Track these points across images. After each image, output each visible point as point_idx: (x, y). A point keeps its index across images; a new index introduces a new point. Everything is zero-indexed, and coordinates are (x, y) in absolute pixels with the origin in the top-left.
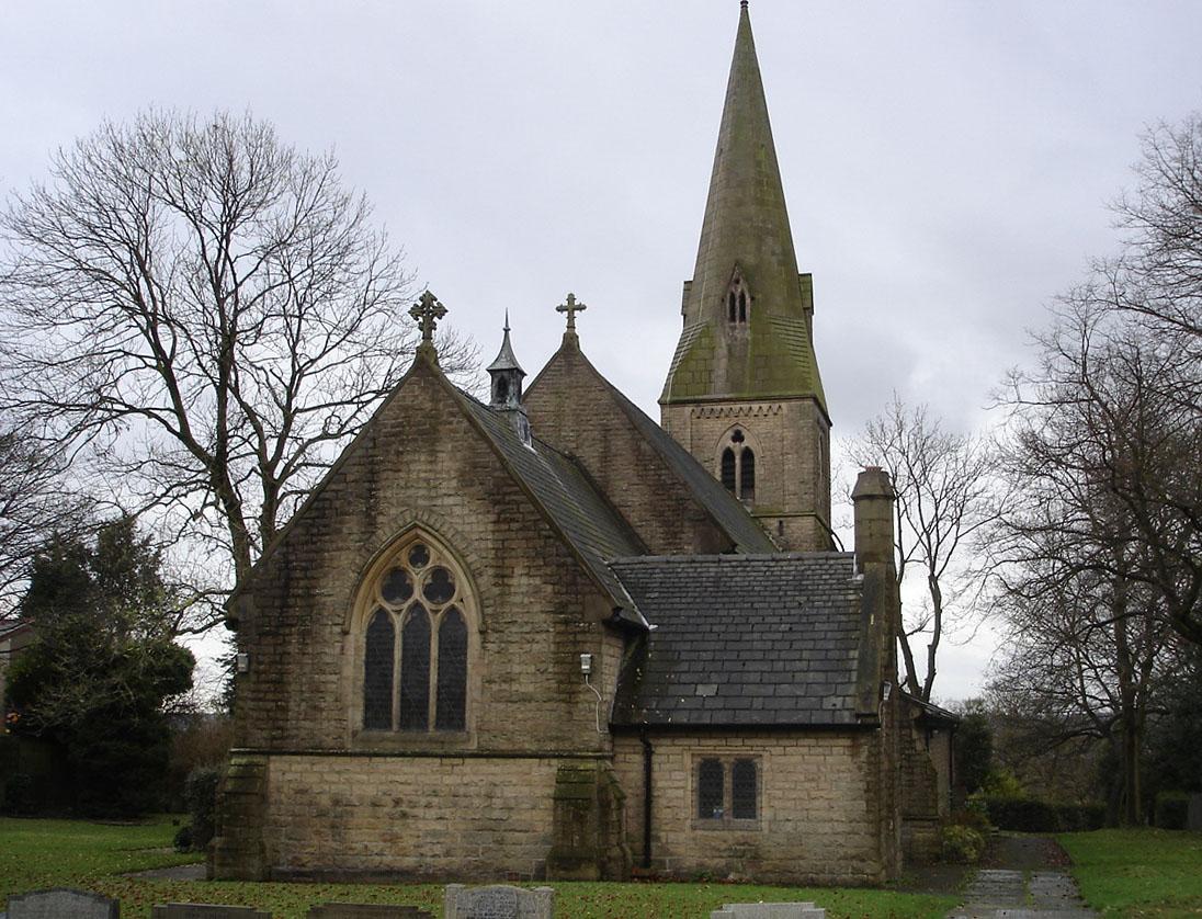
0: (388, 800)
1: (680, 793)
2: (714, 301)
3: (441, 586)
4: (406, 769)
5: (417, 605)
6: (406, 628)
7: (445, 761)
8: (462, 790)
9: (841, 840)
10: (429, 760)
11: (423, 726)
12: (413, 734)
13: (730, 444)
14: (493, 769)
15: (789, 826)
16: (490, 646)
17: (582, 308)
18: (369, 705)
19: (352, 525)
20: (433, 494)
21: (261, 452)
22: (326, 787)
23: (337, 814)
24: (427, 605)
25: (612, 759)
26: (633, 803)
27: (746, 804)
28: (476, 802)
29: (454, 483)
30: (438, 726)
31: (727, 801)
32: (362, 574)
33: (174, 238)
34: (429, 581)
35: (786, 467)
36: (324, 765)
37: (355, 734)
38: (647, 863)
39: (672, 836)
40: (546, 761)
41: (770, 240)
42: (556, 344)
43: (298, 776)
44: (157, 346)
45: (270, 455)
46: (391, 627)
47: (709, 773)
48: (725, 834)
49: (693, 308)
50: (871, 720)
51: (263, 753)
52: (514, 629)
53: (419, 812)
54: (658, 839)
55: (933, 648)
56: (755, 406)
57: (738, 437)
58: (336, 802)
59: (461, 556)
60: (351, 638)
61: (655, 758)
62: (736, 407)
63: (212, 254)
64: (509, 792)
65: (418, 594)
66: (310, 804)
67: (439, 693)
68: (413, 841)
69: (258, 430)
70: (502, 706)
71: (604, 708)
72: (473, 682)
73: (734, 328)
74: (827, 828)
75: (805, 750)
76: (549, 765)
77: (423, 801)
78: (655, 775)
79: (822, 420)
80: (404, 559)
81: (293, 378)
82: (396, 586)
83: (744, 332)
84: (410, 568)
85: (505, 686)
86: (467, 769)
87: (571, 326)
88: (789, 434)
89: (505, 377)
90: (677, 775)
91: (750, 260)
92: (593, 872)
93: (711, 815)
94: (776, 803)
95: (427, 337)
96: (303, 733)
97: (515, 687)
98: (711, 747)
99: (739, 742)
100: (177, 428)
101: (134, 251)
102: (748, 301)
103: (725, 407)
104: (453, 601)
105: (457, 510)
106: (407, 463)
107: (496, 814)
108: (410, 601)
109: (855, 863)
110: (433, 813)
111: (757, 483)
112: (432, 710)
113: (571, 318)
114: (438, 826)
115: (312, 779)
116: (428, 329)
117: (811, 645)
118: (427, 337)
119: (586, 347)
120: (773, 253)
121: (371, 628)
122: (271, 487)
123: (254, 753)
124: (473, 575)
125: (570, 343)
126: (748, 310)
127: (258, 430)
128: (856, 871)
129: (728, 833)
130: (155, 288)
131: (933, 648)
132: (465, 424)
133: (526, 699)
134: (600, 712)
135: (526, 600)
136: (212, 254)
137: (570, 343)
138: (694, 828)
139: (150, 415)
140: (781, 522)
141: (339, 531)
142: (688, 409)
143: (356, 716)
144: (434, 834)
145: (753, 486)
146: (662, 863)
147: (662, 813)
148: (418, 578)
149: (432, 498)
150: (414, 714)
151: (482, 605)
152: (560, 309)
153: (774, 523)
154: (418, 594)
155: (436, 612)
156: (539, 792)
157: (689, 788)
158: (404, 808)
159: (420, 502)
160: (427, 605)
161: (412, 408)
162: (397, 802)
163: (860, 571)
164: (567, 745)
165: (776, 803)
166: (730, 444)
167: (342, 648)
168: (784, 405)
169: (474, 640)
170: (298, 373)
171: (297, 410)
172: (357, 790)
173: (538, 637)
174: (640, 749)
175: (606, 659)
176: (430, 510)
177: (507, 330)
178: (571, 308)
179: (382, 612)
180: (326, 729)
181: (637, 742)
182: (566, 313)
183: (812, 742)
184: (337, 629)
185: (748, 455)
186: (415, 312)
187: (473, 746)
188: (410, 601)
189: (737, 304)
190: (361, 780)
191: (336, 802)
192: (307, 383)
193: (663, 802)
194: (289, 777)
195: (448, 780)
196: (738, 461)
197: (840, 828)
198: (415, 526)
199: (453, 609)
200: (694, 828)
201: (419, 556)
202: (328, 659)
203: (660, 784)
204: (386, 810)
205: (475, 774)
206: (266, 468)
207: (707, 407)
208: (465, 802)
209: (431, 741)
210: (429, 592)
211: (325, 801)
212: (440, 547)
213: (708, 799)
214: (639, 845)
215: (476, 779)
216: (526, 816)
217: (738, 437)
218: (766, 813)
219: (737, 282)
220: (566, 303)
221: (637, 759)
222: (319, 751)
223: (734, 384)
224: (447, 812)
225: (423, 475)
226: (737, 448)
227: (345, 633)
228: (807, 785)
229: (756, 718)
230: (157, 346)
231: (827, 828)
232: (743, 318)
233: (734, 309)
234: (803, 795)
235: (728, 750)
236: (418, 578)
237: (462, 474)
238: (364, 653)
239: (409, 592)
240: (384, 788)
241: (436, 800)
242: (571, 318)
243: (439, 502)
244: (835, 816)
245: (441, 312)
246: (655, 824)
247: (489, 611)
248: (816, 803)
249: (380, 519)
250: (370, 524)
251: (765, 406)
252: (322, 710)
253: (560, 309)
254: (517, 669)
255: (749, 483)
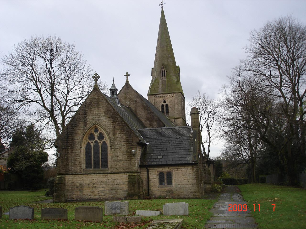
0: (92, 184)
1: (155, 180)
2: (158, 72)
3: (101, 137)
4: (95, 177)
5: (96, 141)
6: (94, 146)
7: (104, 175)
8: (108, 181)
9: (191, 188)
10: (100, 175)
11: (99, 167)
12: (96, 169)
13: (163, 103)
14: (114, 176)
15: (179, 186)
16: (112, 149)
17: (129, 75)
18: (87, 163)
19: (81, 124)
20: (99, 117)
21: (61, 109)
22: (78, 181)
23: (81, 187)
24: (98, 141)
25: (140, 173)
26: (145, 182)
27: (170, 181)
28: (111, 183)
29: (103, 114)
30: (102, 167)
31: (165, 181)
32: (84, 135)
33: (40, 63)
34: (99, 136)
35: (175, 108)
36: (77, 177)
37: (84, 169)
38: (149, 195)
39: (154, 189)
40: (126, 174)
41: (170, 59)
42: (124, 83)
43: (72, 179)
44: (37, 87)
45: (63, 110)
46: (91, 146)
47: (161, 175)
48: (165, 188)
49: (154, 74)
50: (196, 162)
51: (64, 175)
52: (118, 145)
53: (99, 186)
54: (151, 190)
55: (209, 146)
56: (168, 95)
57: (165, 102)
58: (80, 185)
59: (105, 130)
60: (82, 149)
61: (149, 172)
62: (164, 95)
63: (48, 66)
64: (118, 181)
65: (96, 139)
66: (75, 185)
67: (102, 160)
68: (97, 192)
69: (60, 104)
70: (116, 162)
71: (138, 162)
72: (109, 157)
73: (163, 78)
74: (187, 186)
75: (182, 169)
76: (126, 175)
77: (99, 184)
78: (150, 176)
79: (183, 97)
80: (93, 131)
81: (67, 93)
82: (92, 137)
83: (165, 79)
84: (94, 133)
85: (116, 158)
86: (109, 176)
87: (127, 79)
88: (176, 101)
89: (113, 91)
90: (154, 176)
91: (166, 63)
92: (137, 198)
93: (162, 184)
94: (176, 181)
95: (96, 83)
96: (73, 170)
97: (118, 158)
98: (161, 169)
99: (168, 168)
100: (42, 105)
101: (32, 66)
102: (166, 72)
103: (162, 95)
104: (104, 140)
105: (104, 120)
106: (93, 110)
107: (115, 186)
108: (95, 140)
109: (194, 193)
110: (101, 186)
111: (169, 112)
112: (100, 164)
113: (127, 77)
114: (103, 189)
115: (75, 180)
116: (96, 81)
117: (182, 146)
118: (96, 83)
119: (131, 84)
120: (171, 62)
121: (86, 146)
122: (63, 117)
123: (62, 175)
124: (108, 134)
125: (127, 83)
126: (166, 74)
127: (60, 104)
128: (194, 195)
129: (166, 188)
130: (36, 74)
131: (209, 146)
132: (105, 101)
133: (121, 160)
134: (137, 163)
135: (120, 139)
136: (48, 66)
137: (127, 83)
138: (158, 187)
139: (37, 102)
140: (175, 120)
141: (79, 126)
142: (154, 96)
143: (84, 166)
144: (102, 191)
145: (168, 112)
146: (152, 195)
147: (151, 184)
148: (96, 135)
149: (99, 118)
150: (96, 165)
151: (110, 141)
152: (125, 75)
153: (173, 120)
154: (96, 139)
155: (100, 142)
156: (124, 181)
157: (157, 178)
158: (95, 185)
159: (96, 119)
160: (98, 141)
161: (93, 98)
162: (94, 184)
163: (193, 130)
164: (130, 170)
165: (176, 181)
166: (163, 103)
167: (80, 151)
168: (174, 94)
169: (109, 148)
170: (68, 92)
171: (69, 100)
172: (85, 182)
173: (123, 147)
174: (146, 170)
175: (138, 151)
176: (98, 120)
177: (113, 81)
178: (127, 75)
179: (89, 143)
180: (78, 169)
181: (145, 169)
182: (126, 76)
183: (183, 167)
184: (79, 147)
185: (167, 105)
186: (93, 77)
187: (110, 171)
188: (95, 140)
189: (163, 73)
190: (85, 180)
191: (80, 185)
192: (70, 94)
193: (152, 182)
194: (70, 179)
195: (104, 179)
196: (165, 107)
197: (190, 186)
198: (95, 124)
199: (104, 141)
200: (158, 187)
201: (96, 130)
202: (77, 154)
203: (151, 178)
204: (91, 186)
205: (110, 177)
206: (62, 113)
207: (158, 96)
208: (108, 183)
209: (100, 170)
210: (99, 138)
211: (78, 184)
212: (101, 128)
213: (161, 181)
214: (147, 191)
215: (110, 178)
216: (122, 186)
217: (165, 102)
218: (174, 183)
219: (163, 68)
220: (126, 74)
221: (145, 173)
222: (76, 174)
223: (163, 90)
224: (105, 186)
225: (96, 113)
226: (165, 104)
227: (81, 148)
228: (183, 177)
229: (171, 163)
230: (37, 87)
231: (187, 186)
232: (165, 76)
233: (163, 74)
234: (182, 179)
235: (165, 170)
236: (96, 135)
237: (105, 112)
238: (85, 152)
239: (94, 138)
240: (91, 181)
241: (102, 183)
242: (127, 77)
243: (100, 118)
244: (189, 183)
245: (99, 77)
246: (150, 186)
247: (112, 142)
248: (185, 181)
249: (88, 123)
250: (85, 124)
251: (170, 95)
252: (76, 165)
253: (125, 75)
254: (118, 154)
255: (167, 112)
